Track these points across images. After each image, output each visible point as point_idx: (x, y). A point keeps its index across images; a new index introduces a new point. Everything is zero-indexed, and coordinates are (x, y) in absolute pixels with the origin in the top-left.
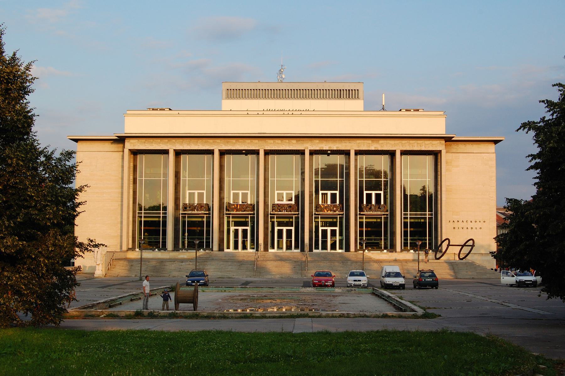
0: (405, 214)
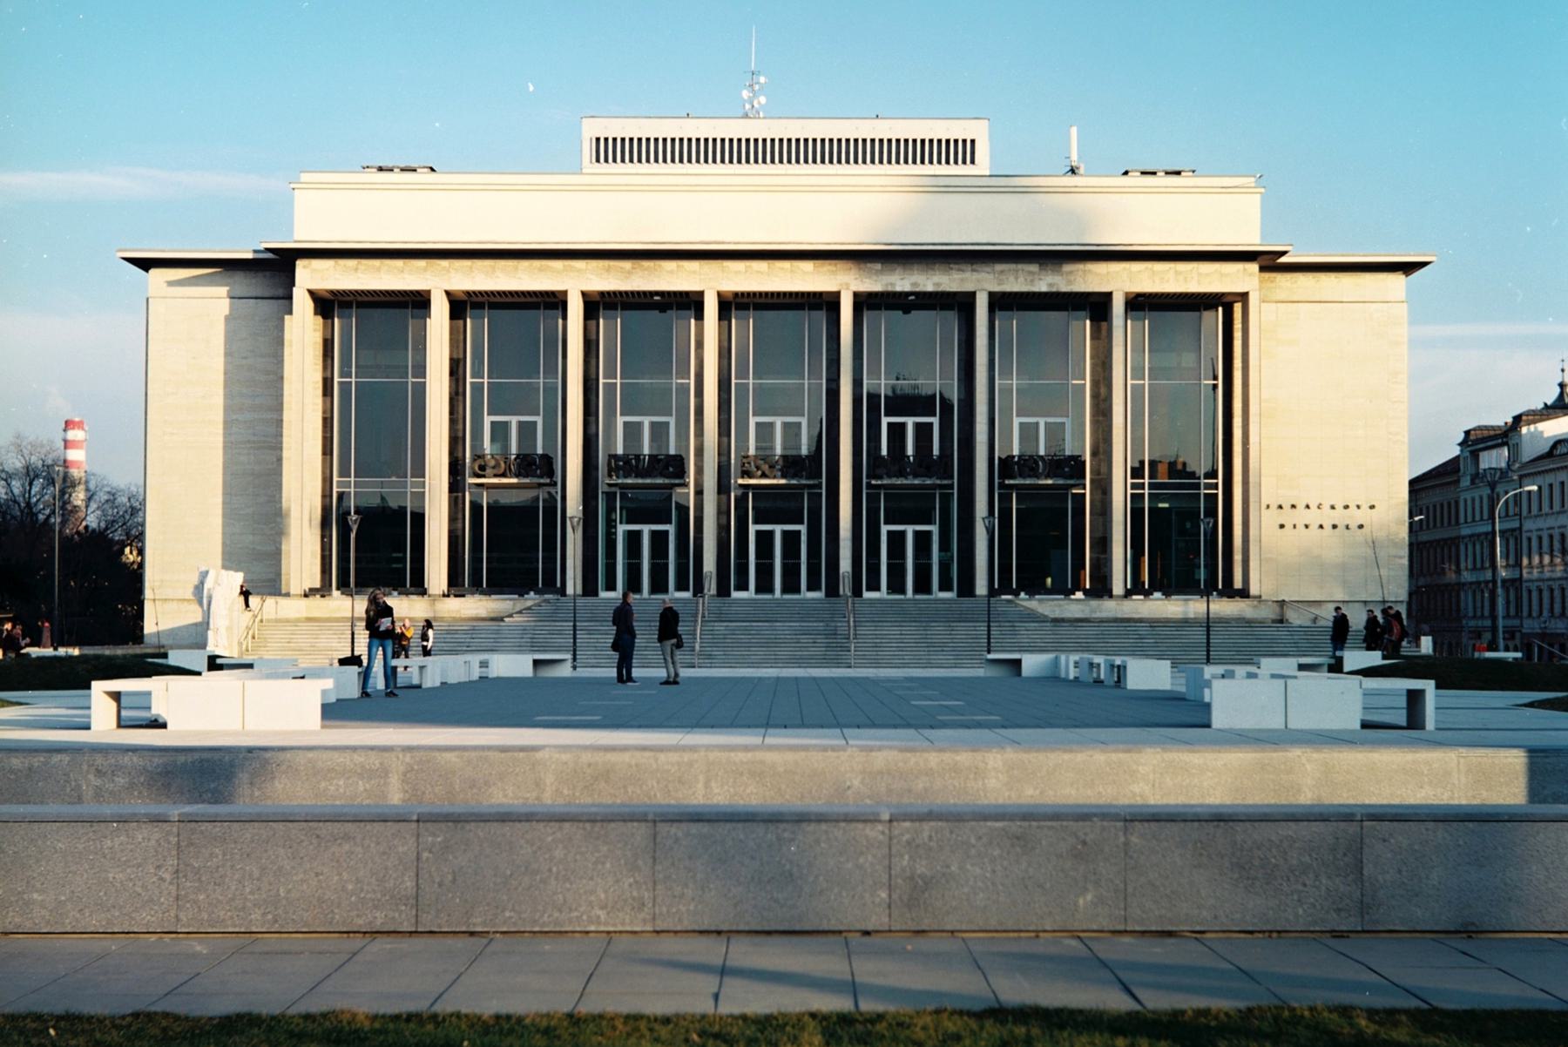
0: (1134, 486)
